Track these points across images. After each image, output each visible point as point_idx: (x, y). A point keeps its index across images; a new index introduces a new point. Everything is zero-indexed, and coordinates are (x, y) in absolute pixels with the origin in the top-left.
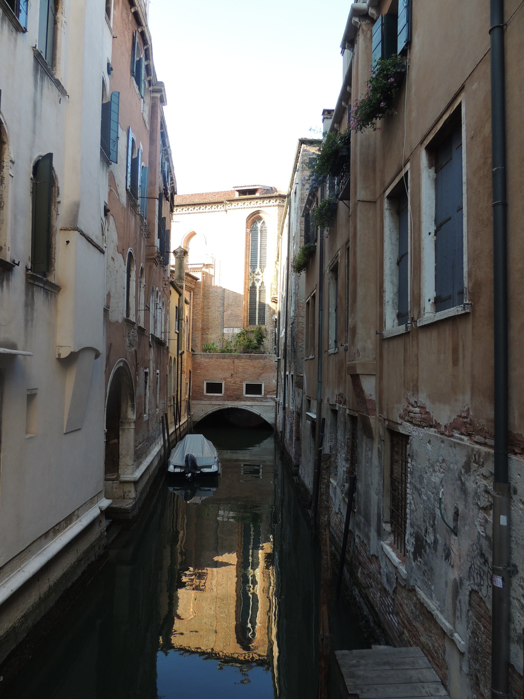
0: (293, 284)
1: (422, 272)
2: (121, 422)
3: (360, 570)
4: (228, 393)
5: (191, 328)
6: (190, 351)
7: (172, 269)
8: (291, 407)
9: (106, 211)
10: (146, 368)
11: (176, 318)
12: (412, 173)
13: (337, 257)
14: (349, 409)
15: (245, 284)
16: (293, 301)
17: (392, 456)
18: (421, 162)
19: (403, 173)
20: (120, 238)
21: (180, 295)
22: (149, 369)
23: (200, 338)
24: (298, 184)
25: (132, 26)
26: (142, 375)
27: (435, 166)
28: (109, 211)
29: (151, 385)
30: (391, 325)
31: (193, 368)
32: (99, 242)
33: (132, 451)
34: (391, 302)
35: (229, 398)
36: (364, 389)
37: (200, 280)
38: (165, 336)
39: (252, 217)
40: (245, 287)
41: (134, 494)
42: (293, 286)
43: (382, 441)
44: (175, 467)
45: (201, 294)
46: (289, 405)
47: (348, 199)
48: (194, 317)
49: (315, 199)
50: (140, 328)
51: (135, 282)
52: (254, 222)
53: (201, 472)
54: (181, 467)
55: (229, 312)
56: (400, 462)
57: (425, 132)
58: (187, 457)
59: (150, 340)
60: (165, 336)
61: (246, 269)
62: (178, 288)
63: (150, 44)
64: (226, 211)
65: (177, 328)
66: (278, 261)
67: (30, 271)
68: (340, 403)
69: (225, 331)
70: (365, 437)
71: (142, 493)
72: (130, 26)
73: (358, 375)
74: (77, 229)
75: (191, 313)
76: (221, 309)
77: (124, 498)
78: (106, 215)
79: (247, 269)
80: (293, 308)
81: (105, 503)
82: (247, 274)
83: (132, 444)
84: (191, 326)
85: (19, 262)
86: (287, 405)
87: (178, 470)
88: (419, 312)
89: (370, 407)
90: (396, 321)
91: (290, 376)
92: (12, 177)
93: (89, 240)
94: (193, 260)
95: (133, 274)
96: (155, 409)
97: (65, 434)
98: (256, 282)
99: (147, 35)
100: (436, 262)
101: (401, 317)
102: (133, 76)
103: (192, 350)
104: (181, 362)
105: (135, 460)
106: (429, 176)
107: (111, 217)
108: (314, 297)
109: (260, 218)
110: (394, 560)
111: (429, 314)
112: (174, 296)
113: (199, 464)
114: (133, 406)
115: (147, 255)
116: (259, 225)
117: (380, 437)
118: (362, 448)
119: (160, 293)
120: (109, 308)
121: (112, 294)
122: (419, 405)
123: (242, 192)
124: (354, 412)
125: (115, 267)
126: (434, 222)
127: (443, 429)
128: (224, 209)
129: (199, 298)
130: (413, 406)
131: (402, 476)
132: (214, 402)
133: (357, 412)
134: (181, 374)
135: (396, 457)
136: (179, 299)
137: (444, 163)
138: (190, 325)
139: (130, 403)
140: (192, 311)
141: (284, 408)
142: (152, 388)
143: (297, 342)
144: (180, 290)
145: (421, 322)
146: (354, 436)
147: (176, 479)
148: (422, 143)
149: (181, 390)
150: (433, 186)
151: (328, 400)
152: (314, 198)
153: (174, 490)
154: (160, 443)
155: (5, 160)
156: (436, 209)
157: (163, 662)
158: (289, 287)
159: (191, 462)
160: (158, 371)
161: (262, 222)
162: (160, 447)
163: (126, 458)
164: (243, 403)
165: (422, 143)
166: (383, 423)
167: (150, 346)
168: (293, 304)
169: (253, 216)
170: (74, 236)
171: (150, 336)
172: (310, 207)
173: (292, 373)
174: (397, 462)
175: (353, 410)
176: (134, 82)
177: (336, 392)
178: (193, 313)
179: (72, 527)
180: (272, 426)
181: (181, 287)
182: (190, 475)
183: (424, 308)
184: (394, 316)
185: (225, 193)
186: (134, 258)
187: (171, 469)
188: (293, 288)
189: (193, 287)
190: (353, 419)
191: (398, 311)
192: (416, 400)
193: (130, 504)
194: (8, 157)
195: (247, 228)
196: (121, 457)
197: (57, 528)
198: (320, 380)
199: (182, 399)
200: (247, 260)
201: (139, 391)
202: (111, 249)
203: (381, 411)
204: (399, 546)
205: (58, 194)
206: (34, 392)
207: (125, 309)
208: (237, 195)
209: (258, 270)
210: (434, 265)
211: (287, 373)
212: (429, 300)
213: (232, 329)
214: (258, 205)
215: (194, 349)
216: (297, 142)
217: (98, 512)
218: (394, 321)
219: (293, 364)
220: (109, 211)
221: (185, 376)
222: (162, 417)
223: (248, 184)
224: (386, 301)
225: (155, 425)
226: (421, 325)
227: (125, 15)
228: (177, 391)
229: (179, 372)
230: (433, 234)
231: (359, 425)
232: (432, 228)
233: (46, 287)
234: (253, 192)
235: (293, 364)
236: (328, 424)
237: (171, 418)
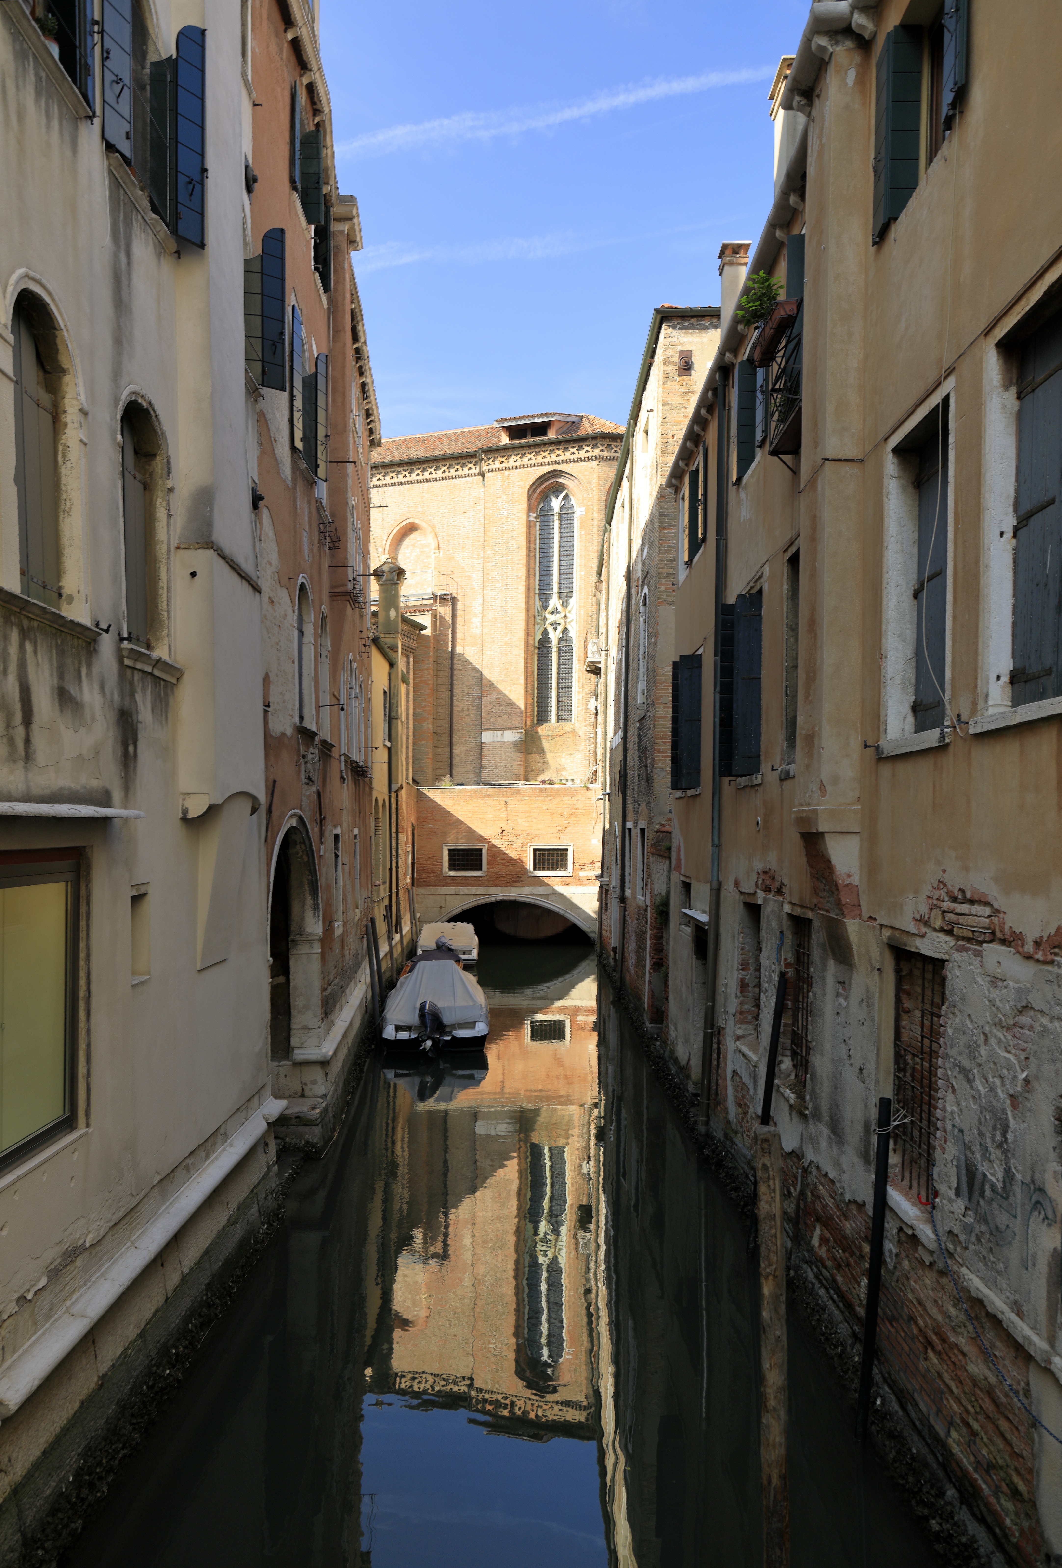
0: (642, 632)
1: (981, 618)
2: (293, 941)
3: (818, 1232)
4: (495, 870)
5: (411, 734)
6: (411, 782)
7: (373, 608)
8: (638, 897)
9: (256, 500)
10: (335, 826)
11: (385, 715)
13: (760, 577)
14: (790, 903)
15: (528, 634)
16: (643, 669)
17: (898, 1001)
18: (984, 375)
19: (935, 400)
20: (282, 555)
21: (392, 665)
22: (341, 828)
23: (430, 756)
24: (652, 411)
25: (286, 72)
26: (330, 841)
27: (1017, 384)
28: (261, 498)
29: (346, 860)
30: (898, 726)
31: (418, 818)
32: (248, 567)
33: (316, 999)
34: (898, 680)
35: (496, 880)
36: (833, 862)
37: (427, 632)
38: (366, 755)
39: (534, 491)
40: (527, 642)
41: (323, 1088)
42: (642, 636)
44: (398, 1028)
45: (431, 660)
46: (634, 894)
47: (796, 451)
48: (418, 710)
49: (701, 449)
50: (324, 742)
51: (312, 647)
52: (545, 497)
53: (453, 1037)
54: (409, 1028)
56: (918, 1014)
57: (996, 311)
58: (422, 1007)
59: (343, 768)
60: (366, 755)
61: (528, 602)
62: (388, 650)
63: (326, 110)
64: (482, 474)
65: (387, 738)
66: (600, 581)
67: (126, 642)
68: (767, 890)
69: (487, 737)
71: (336, 1083)
72: (286, 74)
73: (823, 833)
74: (210, 545)
75: (411, 703)
76: (476, 690)
77: (303, 1096)
78: (255, 507)
79: (531, 602)
80: (641, 686)
81: (274, 1107)
82: (531, 612)
83: (317, 984)
84: (411, 730)
85: (110, 626)
86: (628, 893)
87: (404, 1035)
88: (975, 703)
89: (845, 899)
90: (910, 719)
91: (636, 833)
92: (85, 444)
93: (234, 567)
94: (414, 590)
95: (309, 629)
96: (354, 911)
97: (199, 971)
98: (550, 629)
99: (322, 92)
100: (1014, 596)
101: (926, 711)
102: (295, 188)
103: (414, 780)
104: (397, 809)
105: (322, 1019)
106: (1004, 407)
107: (265, 511)
109: (558, 489)
110: (906, 1212)
111: (997, 705)
112: (379, 667)
113: (447, 1019)
114: (316, 907)
115: (333, 587)
116: (556, 503)
118: (824, 984)
119: (355, 665)
120: (269, 706)
121: (272, 676)
122: (968, 896)
123: (516, 432)
124: (805, 910)
125: (275, 618)
126: (1011, 509)
127: (1029, 948)
128: (477, 471)
129: (428, 669)
130: (954, 900)
131: (922, 1043)
132: (464, 890)
133: (812, 910)
134: (397, 832)
135: (907, 1004)
136: (389, 675)
137: (1038, 379)
138: (408, 728)
139: (309, 901)
140: (411, 697)
141: (623, 899)
142: (347, 868)
143: (653, 760)
144: (391, 654)
145: (979, 725)
146: (802, 958)
147: (404, 1055)
148: (987, 332)
149: (397, 867)
150: (1012, 430)
151: (737, 884)
152: (697, 446)
153: (397, 1075)
154: (363, 980)
155: (68, 409)
156: (1017, 480)
157: (378, 1418)
158: (632, 639)
159: (431, 1020)
160: (356, 831)
161: (562, 496)
162: (364, 988)
163: (306, 1013)
164: (527, 889)
165: (987, 332)
166: (878, 932)
167: (343, 779)
168: (642, 677)
169: (541, 483)
170: (202, 559)
171: (343, 758)
172: (687, 465)
173: (642, 825)
174: (908, 1011)
175: (802, 906)
176: (298, 203)
178: (414, 701)
179: (217, 1158)
180: (592, 935)
181: (394, 649)
182: (429, 1043)
183: (987, 695)
184: (907, 709)
185: (478, 435)
186: (310, 596)
187: (389, 1033)
188: (642, 642)
189: (414, 645)
190: (800, 925)
191: (913, 698)
194: (74, 402)
195: (530, 509)
196: (294, 1012)
197: (189, 1161)
198: (716, 842)
199: (401, 884)
200: (532, 581)
201: (324, 872)
202: (266, 582)
204: (915, 1184)
205: (169, 471)
206: (143, 890)
207: (297, 706)
208: (505, 440)
209: (554, 602)
210: (1011, 601)
211: (629, 825)
212: (998, 678)
213: (500, 732)
214: (554, 457)
215: (416, 779)
216: (649, 318)
217: (264, 1126)
218: (905, 718)
219: (643, 805)
220: (261, 498)
221: (405, 837)
222: (366, 926)
223: (529, 410)
224: (889, 676)
225: (355, 944)
226: (978, 730)
227: (273, 48)
228: (391, 869)
229: (394, 830)
230: (1009, 534)
231: (818, 937)
232: (1009, 521)
233: (157, 673)
234: (541, 429)
235: (643, 805)
237: (382, 927)
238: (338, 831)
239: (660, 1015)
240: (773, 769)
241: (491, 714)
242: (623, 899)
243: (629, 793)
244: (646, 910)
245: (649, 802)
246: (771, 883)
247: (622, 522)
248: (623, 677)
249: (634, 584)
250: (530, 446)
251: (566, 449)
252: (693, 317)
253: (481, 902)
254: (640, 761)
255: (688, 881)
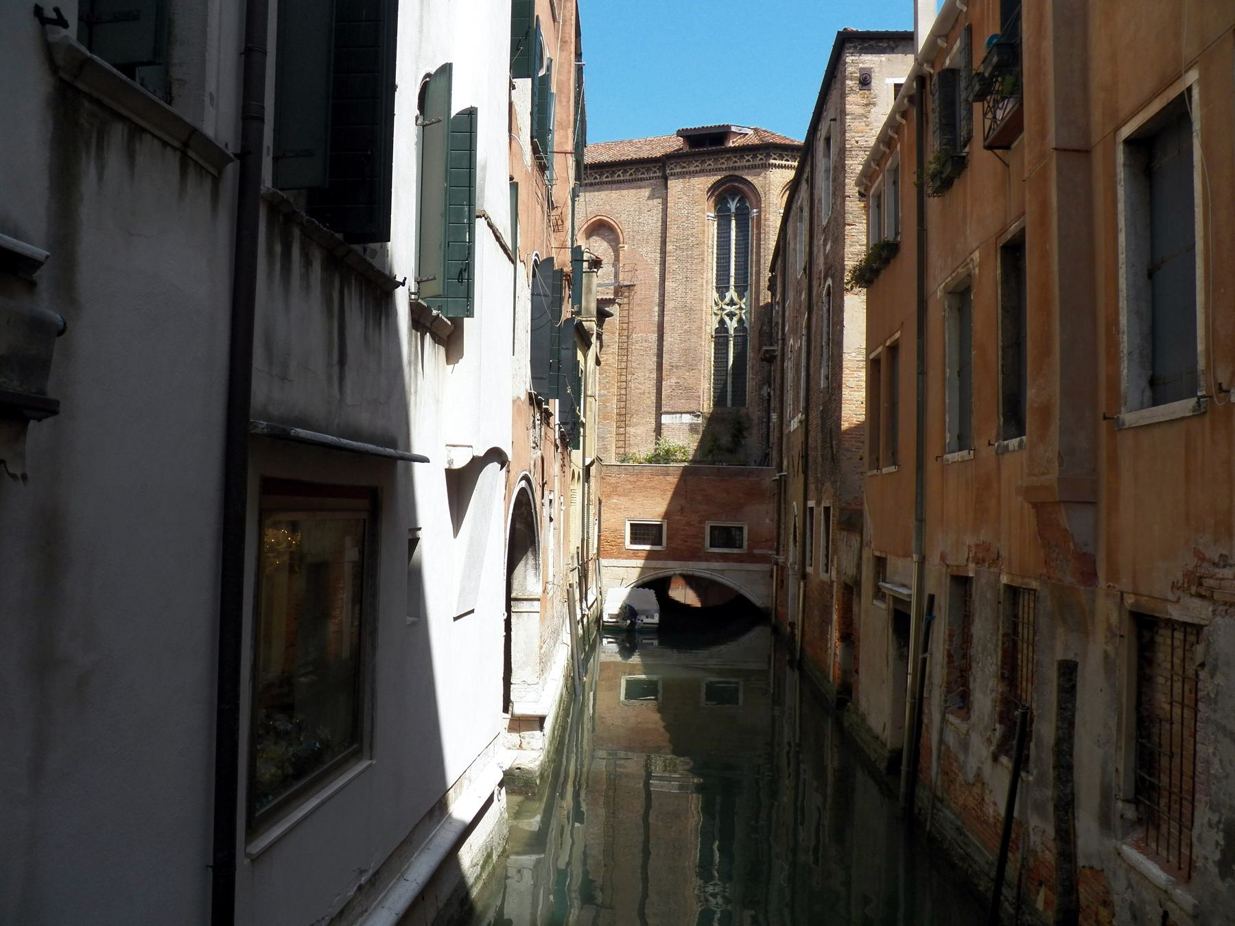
12: (1205, 102)
19: (1172, 93)
24: (834, 120)
39: (719, 187)
43: (1111, 633)
46: (816, 569)
55: (674, 380)
70: (1060, 630)
98: (727, 319)
108: (893, 349)
117: (1109, 629)
151: (943, 558)
164: (704, 565)
177: (969, 540)
192: (1225, 552)
193: (535, 760)
203: (1113, 575)
211: (811, 503)
218: (1143, 392)
219: (828, 484)
235: (828, 484)
236: (943, 604)
238: (551, 497)
239: (847, 690)
240: (990, 444)
241: (670, 397)
242: (804, 576)
243: (810, 473)
244: (831, 586)
245: (835, 482)
246: (986, 556)
247: (801, 220)
248: (803, 363)
249: (815, 276)
250: (708, 153)
251: (742, 157)
252: (872, 39)
253: (661, 575)
254: (824, 441)
255: (883, 555)
